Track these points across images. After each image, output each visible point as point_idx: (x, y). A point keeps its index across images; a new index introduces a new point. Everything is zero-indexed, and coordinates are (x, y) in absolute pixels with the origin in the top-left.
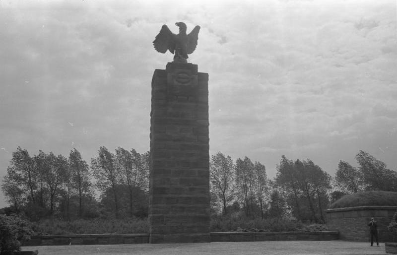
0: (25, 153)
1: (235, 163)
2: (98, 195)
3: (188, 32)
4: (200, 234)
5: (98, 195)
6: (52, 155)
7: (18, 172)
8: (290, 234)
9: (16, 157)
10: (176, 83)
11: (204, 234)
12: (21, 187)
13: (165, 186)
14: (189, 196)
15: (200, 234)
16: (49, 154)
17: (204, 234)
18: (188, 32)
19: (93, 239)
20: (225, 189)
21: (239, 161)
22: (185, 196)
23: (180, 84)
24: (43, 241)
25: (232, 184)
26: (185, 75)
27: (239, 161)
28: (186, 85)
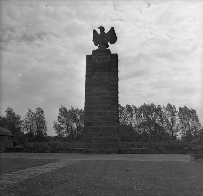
0: (64, 108)
1: (178, 110)
2: (179, 136)
3: (106, 31)
4: (112, 149)
5: (179, 136)
6: (78, 109)
7: (62, 118)
8: (173, 150)
9: (61, 110)
10: (97, 61)
11: (114, 149)
12: (62, 126)
13: (91, 121)
14: (105, 127)
15: (112, 149)
16: (76, 109)
17: (114, 149)
18: (106, 31)
19: (55, 150)
20: (172, 125)
21: (181, 109)
22: (103, 127)
23: (99, 62)
24: (32, 150)
25: (178, 122)
26: (103, 56)
27: (181, 109)
28: (103, 62)
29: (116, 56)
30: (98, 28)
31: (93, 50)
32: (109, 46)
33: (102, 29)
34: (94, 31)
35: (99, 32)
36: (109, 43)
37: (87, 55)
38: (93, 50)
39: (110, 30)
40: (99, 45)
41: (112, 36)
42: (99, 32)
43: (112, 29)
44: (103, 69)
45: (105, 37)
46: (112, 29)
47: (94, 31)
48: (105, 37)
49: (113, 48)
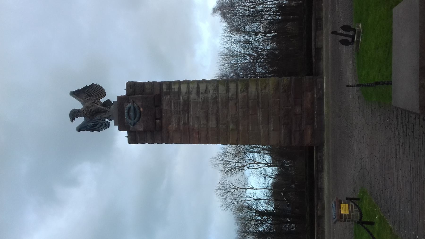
3: (79, 106)
18: (79, 106)
23: (142, 116)
29: (133, 88)
30: (72, 122)
31: (129, 143)
32: (109, 101)
33: (74, 115)
34: (80, 129)
35: (80, 120)
36: (103, 100)
37: (129, 142)
38: (129, 143)
39: (153, 84)
40: (107, 120)
41: (90, 94)
42: (80, 120)
43: (76, 94)
44: (156, 108)
45: (93, 110)
46: (76, 94)
47: (80, 129)
48: (93, 110)
49: (115, 91)
